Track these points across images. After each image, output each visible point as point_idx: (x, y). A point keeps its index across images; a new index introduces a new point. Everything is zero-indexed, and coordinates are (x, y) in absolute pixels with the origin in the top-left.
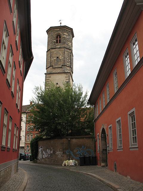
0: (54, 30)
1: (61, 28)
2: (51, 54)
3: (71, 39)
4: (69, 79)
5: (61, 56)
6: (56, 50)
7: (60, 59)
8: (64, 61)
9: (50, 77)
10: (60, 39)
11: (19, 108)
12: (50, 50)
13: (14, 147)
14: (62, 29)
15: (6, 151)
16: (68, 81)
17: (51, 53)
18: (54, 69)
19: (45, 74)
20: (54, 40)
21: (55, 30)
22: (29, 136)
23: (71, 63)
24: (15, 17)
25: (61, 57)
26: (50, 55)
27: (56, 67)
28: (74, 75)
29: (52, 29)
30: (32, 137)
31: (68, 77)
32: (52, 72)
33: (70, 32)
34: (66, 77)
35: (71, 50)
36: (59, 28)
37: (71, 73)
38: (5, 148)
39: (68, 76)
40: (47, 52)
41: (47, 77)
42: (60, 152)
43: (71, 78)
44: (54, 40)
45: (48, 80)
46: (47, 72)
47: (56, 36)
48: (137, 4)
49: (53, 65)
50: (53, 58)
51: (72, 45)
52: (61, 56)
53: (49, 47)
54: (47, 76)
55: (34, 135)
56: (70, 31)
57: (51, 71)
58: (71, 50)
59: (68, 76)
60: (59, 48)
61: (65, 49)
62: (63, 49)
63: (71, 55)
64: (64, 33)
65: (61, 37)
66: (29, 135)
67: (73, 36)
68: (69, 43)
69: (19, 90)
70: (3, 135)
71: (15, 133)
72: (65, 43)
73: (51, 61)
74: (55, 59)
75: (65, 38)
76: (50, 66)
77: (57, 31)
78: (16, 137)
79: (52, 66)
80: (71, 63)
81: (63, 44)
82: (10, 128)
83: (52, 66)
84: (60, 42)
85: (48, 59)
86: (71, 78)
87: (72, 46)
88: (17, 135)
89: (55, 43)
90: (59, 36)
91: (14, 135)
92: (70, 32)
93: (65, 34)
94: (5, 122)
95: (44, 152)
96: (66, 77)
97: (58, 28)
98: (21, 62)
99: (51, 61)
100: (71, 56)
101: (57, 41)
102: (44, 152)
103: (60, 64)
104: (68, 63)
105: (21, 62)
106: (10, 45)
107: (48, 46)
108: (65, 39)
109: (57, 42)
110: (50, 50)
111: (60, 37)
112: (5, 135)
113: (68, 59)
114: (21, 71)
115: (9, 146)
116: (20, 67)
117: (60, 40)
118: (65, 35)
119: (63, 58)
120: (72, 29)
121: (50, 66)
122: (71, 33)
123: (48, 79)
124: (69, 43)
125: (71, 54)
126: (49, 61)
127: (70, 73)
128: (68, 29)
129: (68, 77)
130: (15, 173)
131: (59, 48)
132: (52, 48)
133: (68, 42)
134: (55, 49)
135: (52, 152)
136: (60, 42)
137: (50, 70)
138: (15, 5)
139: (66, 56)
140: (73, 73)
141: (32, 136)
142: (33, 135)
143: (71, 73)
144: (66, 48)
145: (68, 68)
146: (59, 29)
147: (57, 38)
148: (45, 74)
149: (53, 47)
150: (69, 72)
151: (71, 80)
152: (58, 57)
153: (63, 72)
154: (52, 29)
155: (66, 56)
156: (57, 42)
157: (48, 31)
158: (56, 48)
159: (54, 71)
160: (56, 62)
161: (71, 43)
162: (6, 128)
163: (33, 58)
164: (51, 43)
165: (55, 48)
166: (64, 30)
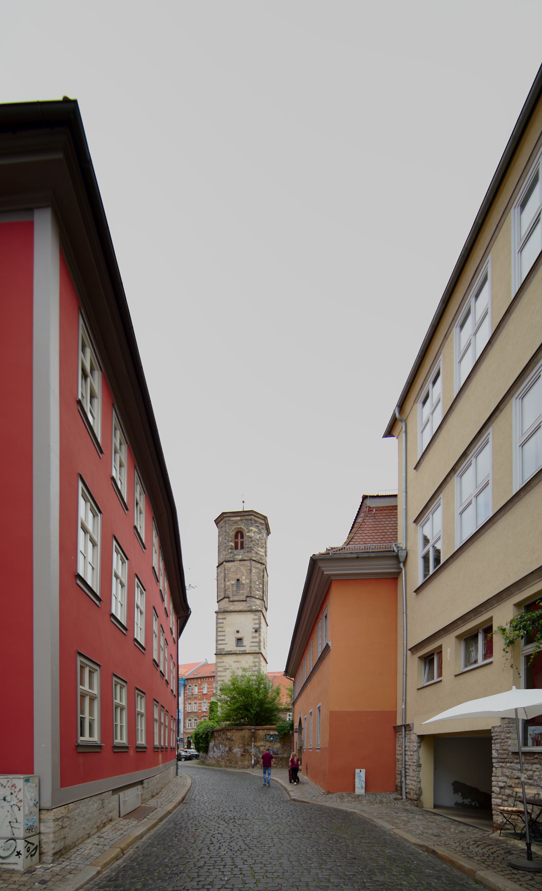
0: (229, 518)
1: (243, 516)
2: (225, 574)
3: (264, 541)
4: (260, 623)
5: (244, 578)
6: (236, 563)
7: (243, 584)
8: (250, 587)
9: (225, 619)
10: (242, 540)
11: (174, 693)
12: (222, 563)
13: (172, 745)
14: (246, 517)
15: (164, 751)
16: (257, 626)
17: (225, 570)
18: (231, 603)
19: (216, 612)
21: (232, 519)
22: (190, 720)
23: (263, 592)
24: (156, 552)
25: (244, 580)
26: (222, 575)
27: (236, 598)
28: (268, 615)
29: (226, 517)
30: (196, 722)
31: (256, 619)
32: (229, 609)
33: (262, 524)
34: (254, 619)
35: (264, 564)
36: (240, 516)
37: (264, 611)
38: (158, 748)
39: (257, 617)
40: (217, 567)
41: (220, 619)
42: (239, 749)
43: (263, 621)
44: (231, 541)
45: (221, 625)
46: (220, 609)
47: (234, 533)
48: (325, 573)
49: (230, 594)
50: (229, 580)
51: (266, 552)
53: (221, 556)
54: (220, 617)
55: (200, 719)
56: (263, 522)
57: (225, 608)
58: (264, 564)
59: (257, 617)
60: (240, 560)
61: (253, 563)
62: (248, 563)
63: (263, 576)
64: (251, 528)
65: (244, 537)
66: (191, 719)
67: (268, 533)
68: (260, 549)
69: (165, 645)
70: (154, 733)
71: (172, 727)
73: (225, 587)
74: (233, 582)
75: (251, 538)
76: (224, 598)
77: (236, 522)
78: (174, 731)
79: (228, 597)
80: (263, 592)
81: (248, 552)
82: (167, 724)
83: (228, 597)
84: (242, 548)
85: (219, 582)
86: (263, 621)
87: (266, 555)
88: (174, 729)
89: (231, 549)
90: (239, 534)
91: (171, 729)
92: (262, 524)
93: (252, 530)
94: (156, 716)
95: (215, 749)
96: (254, 619)
97: (238, 516)
98: (159, 570)
99: (225, 587)
100: (263, 578)
101: (236, 544)
102: (215, 749)
103: (245, 592)
104: (258, 593)
105: (165, 589)
106: (170, 655)
107: (219, 556)
108: (252, 541)
109: (236, 548)
110: (222, 563)
111: (242, 537)
112: (157, 732)
113: (257, 583)
114: (174, 638)
115: (167, 745)
116: (163, 601)
117: (242, 543)
118: (252, 532)
119: (248, 581)
120: (265, 518)
121: (224, 598)
122: (264, 527)
123: (220, 623)
125: (263, 572)
126: (223, 586)
127: (261, 611)
128: (258, 517)
129: (256, 619)
130: (174, 777)
131: (240, 560)
132: (226, 559)
133: (258, 547)
134: (231, 561)
135: (227, 749)
136: (242, 548)
137: (225, 604)
138: (154, 533)
139: (255, 578)
140: (266, 609)
141: (196, 720)
142: (197, 719)
143: (264, 611)
144: (254, 560)
145: (258, 602)
146: (239, 518)
147: (236, 537)
148: (216, 612)
149: (228, 557)
150: (259, 609)
151: (263, 625)
152: (238, 580)
153: (249, 609)
154: (226, 517)
155: (255, 578)
156: (236, 548)
157: (217, 521)
158: (234, 561)
159: (232, 608)
160: (235, 589)
161: (263, 550)
162: (157, 723)
163: (191, 612)
164: (225, 550)
165: (232, 559)
166: (251, 520)
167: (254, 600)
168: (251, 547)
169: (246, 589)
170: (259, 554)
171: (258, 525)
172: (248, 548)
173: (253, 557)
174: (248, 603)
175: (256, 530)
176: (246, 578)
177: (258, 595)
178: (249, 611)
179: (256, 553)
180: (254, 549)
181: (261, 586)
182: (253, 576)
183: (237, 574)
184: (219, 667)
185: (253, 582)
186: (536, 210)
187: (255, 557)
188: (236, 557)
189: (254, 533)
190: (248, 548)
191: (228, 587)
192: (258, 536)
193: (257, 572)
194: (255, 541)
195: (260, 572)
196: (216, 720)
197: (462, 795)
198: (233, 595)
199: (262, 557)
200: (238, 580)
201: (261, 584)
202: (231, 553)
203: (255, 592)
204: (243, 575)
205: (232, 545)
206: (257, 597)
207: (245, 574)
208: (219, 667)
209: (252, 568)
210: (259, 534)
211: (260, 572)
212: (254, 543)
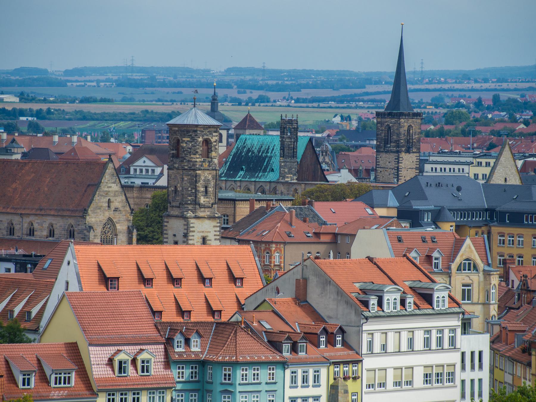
16: (186, 231)
20: (172, 152)
44: (173, 150)
52: (179, 185)
68: (192, 156)
72: (185, 159)
73: (168, 193)
74: (173, 189)
89: (173, 157)
93: (184, 141)
99: (168, 193)
104: (190, 198)
108: (184, 151)
113: (190, 189)
124: (192, 156)
146: (177, 129)
167: (186, 206)
168: (183, 157)
169: (180, 196)
170: (191, 161)
171: (191, 133)
172: (181, 157)
173: (185, 165)
174: (180, 210)
175: (189, 139)
176: (180, 186)
177: (190, 200)
178: (181, 217)
179: (189, 161)
180: (186, 158)
181: (193, 191)
182: (186, 183)
183: (175, 181)
184: (218, 235)
185: (185, 189)
186: (474, 295)
187: (187, 166)
188: (175, 165)
189: (186, 143)
190: (181, 157)
191: (170, 193)
192: (191, 145)
193: (189, 179)
194: (187, 151)
195: (193, 178)
196: (262, 260)
197: (499, 98)
198: (173, 201)
199: (195, 163)
200: (39, 188)
201: (194, 189)
202: (172, 161)
203: (187, 198)
204: (178, 183)
205: (173, 153)
206: (189, 202)
207: (180, 182)
208: (218, 235)
209: (184, 176)
210: (191, 142)
211: (193, 178)
212: (186, 152)
